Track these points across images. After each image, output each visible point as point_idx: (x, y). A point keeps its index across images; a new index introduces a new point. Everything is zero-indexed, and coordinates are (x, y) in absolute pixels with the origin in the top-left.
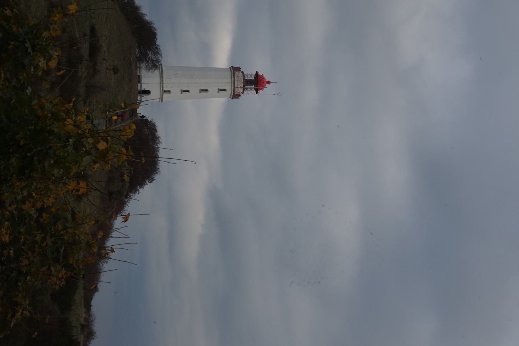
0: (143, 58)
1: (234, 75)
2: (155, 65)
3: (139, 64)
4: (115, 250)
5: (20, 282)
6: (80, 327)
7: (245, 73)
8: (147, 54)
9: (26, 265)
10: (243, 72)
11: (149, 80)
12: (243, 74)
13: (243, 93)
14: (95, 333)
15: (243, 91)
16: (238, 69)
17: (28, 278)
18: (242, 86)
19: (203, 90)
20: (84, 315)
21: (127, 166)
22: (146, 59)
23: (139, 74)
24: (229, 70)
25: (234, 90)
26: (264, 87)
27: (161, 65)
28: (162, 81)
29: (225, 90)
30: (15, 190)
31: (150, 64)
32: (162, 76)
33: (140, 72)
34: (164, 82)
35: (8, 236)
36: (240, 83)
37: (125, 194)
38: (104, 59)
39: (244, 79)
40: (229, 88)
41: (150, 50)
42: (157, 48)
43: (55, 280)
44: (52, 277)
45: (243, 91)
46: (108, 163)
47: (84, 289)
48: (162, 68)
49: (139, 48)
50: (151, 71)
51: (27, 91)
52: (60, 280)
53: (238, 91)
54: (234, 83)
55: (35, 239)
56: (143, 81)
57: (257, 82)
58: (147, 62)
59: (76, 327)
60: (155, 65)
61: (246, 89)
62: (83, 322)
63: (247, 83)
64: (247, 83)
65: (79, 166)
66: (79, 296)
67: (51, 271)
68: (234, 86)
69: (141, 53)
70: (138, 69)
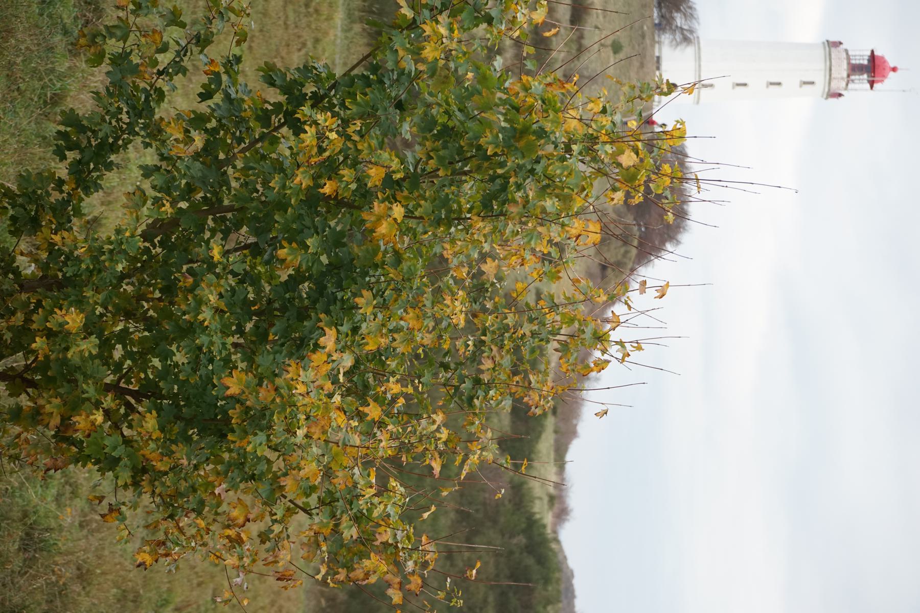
0: (665, 24)
1: (830, 55)
2: (686, 38)
3: (659, 36)
4: (643, 346)
5: (478, 398)
6: (546, 499)
7: (850, 53)
8: (673, 18)
9: (488, 370)
10: (846, 51)
11: (675, 63)
12: (847, 54)
14: (571, 510)
15: (847, 85)
16: (838, 44)
17: (492, 393)
18: (845, 75)
20: (554, 478)
22: (671, 28)
23: (657, 54)
24: (822, 46)
25: (830, 83)
26: (884, 76)
27: (698, 37)
28: (700, 66)
30: (476, 236)
31: (678, 36)
32: (700, 58)
33: (660, 49)
35: (463, 315)
36: (841, 70)
38: (596, 27)
39: (849, 63)
40: (820, 79)
42: (690, 8)
44: (531, 393)
45: (847, 85)
46: (639, 192)
47: (556, 432)
48: (699, 43)
49: (659, 6)
50: (679, 48)
51: (495, 63)
52: (545, 398)
53: (838, 85)
54: (830, 70)
57: (873, 68)
58: (673, 32)
59: (540, 498)
61: (853, 81)
62: (551, 490)
63: (855, 69)
64: (855, 69)
65: (587, 195)
66: (546, 444)
67: (530, 383)
68: (830, 75)
69: (662, 16)
70: (657, 46)
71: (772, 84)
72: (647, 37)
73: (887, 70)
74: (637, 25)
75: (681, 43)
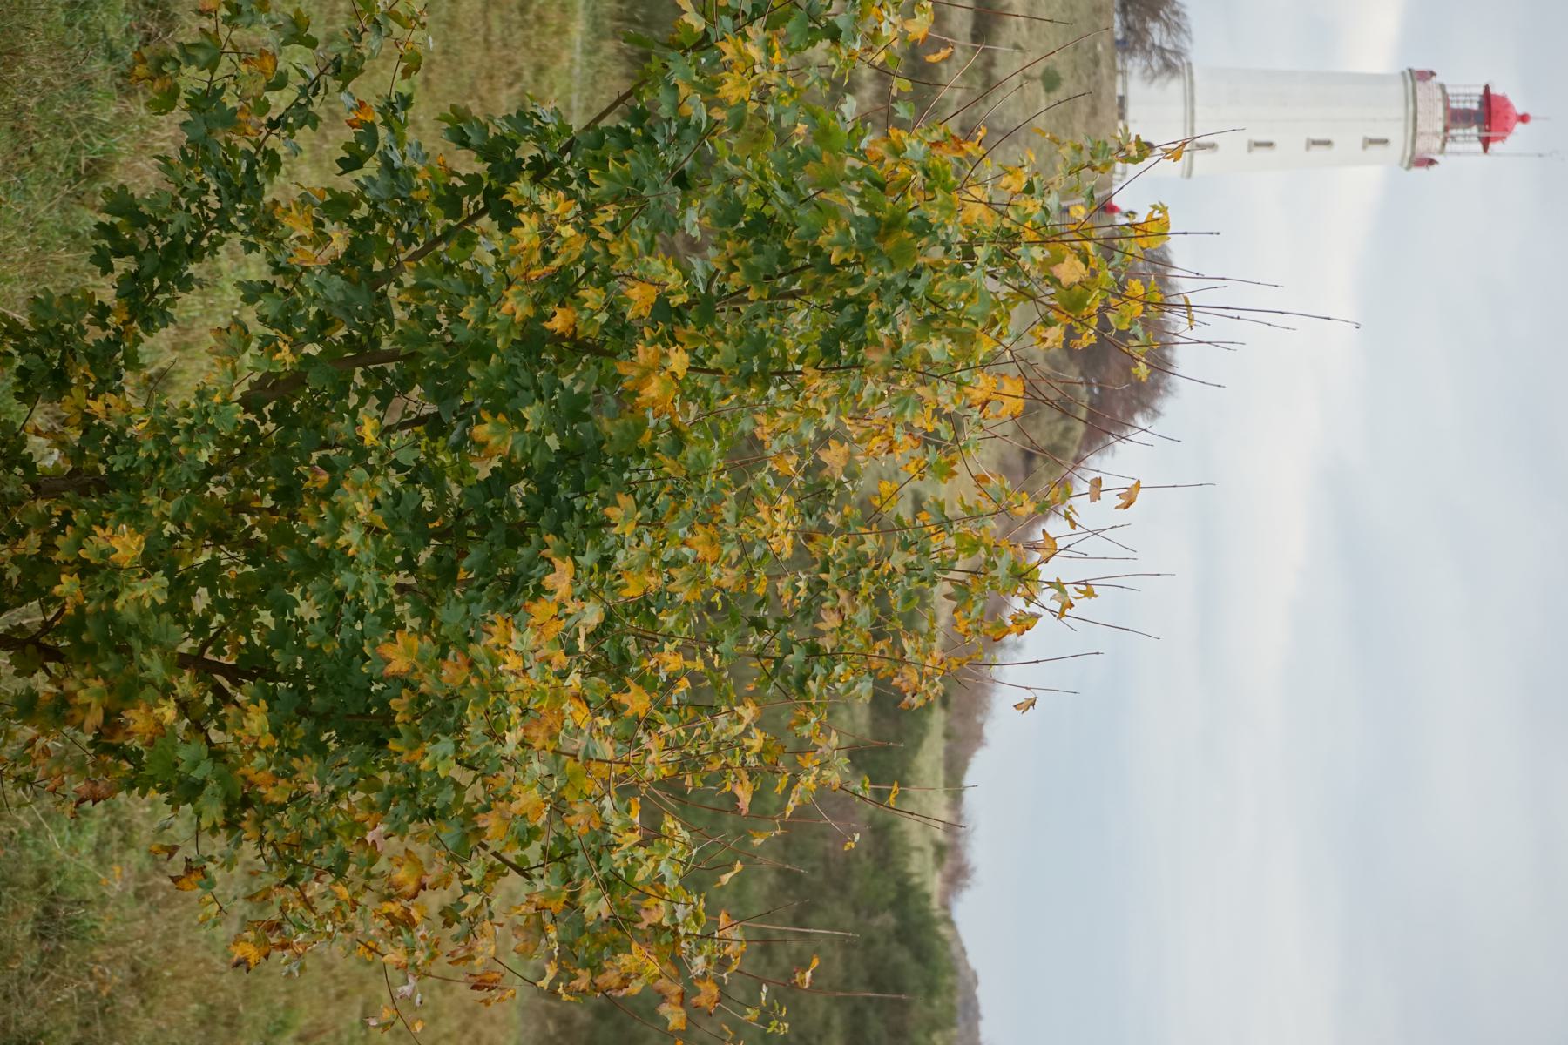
0: (1133, 41)
1: (1414, 93)
2: (1170, 65)
5: (814, 679)
6: (930, 851)
7: (1449, 90)
9: (832, 630)
11: (1150, 107)
12: (1444, 92)
13: (1442, 151)
14: (974, 870)
17: (838, 669)
19: (1373, 142)
20: (944, 815)
21: (1141, 334)
22: (1143, 48)
23: (1119, 92)
25: (1414, 142)
26: (1507, 130)
27: (1190, 64)
28: (1193, 112)
29: (1385, 142)
31: (1156, 62)
32: (1192, 98)
33: (1125, 83)
34: (1198, 116)
35: (790, 537)
36: (1434, 119)
37: (1073, 453)
38: (1016, 46)
39: (1447, 108)
41: (1156, 17)
42: (1176, 13)
43: (916, 679)
44: (905, 669)
47: (947, 736)
48: (1191, 74)
49: (1124, 10)
50: (1157, 82)
51: (844, 108)
52: (929, 678)
53: (1428, 145)
54: (1415, 119)
55: (861, 548)
56: (1132, 112)
59: (920, 849)
60: (1170, 65)
62: (940, 835)
63: (1457, 118)
64: (1457, 118)
65: (1000, 333)
66: (930, 757)
67: (903, 653)
69: (1129, 28)
70: (1119, 78)
71: (1258, 144)
72: (1103, 63)
73: (1512, 119)
74: (1085, 43)
75: (1160, 73)
